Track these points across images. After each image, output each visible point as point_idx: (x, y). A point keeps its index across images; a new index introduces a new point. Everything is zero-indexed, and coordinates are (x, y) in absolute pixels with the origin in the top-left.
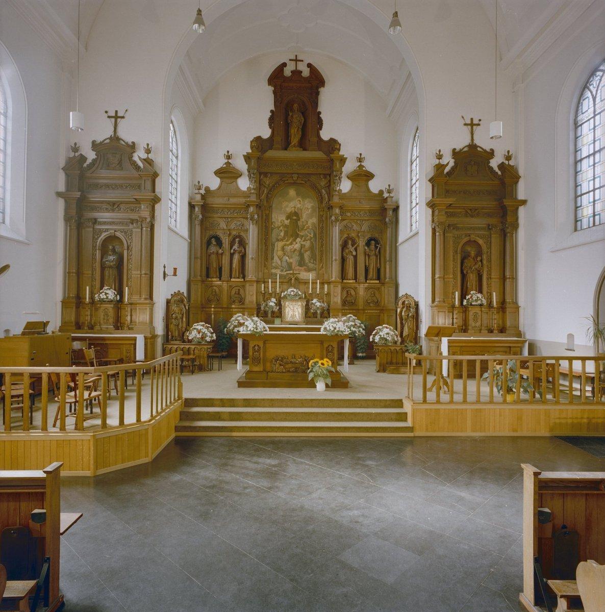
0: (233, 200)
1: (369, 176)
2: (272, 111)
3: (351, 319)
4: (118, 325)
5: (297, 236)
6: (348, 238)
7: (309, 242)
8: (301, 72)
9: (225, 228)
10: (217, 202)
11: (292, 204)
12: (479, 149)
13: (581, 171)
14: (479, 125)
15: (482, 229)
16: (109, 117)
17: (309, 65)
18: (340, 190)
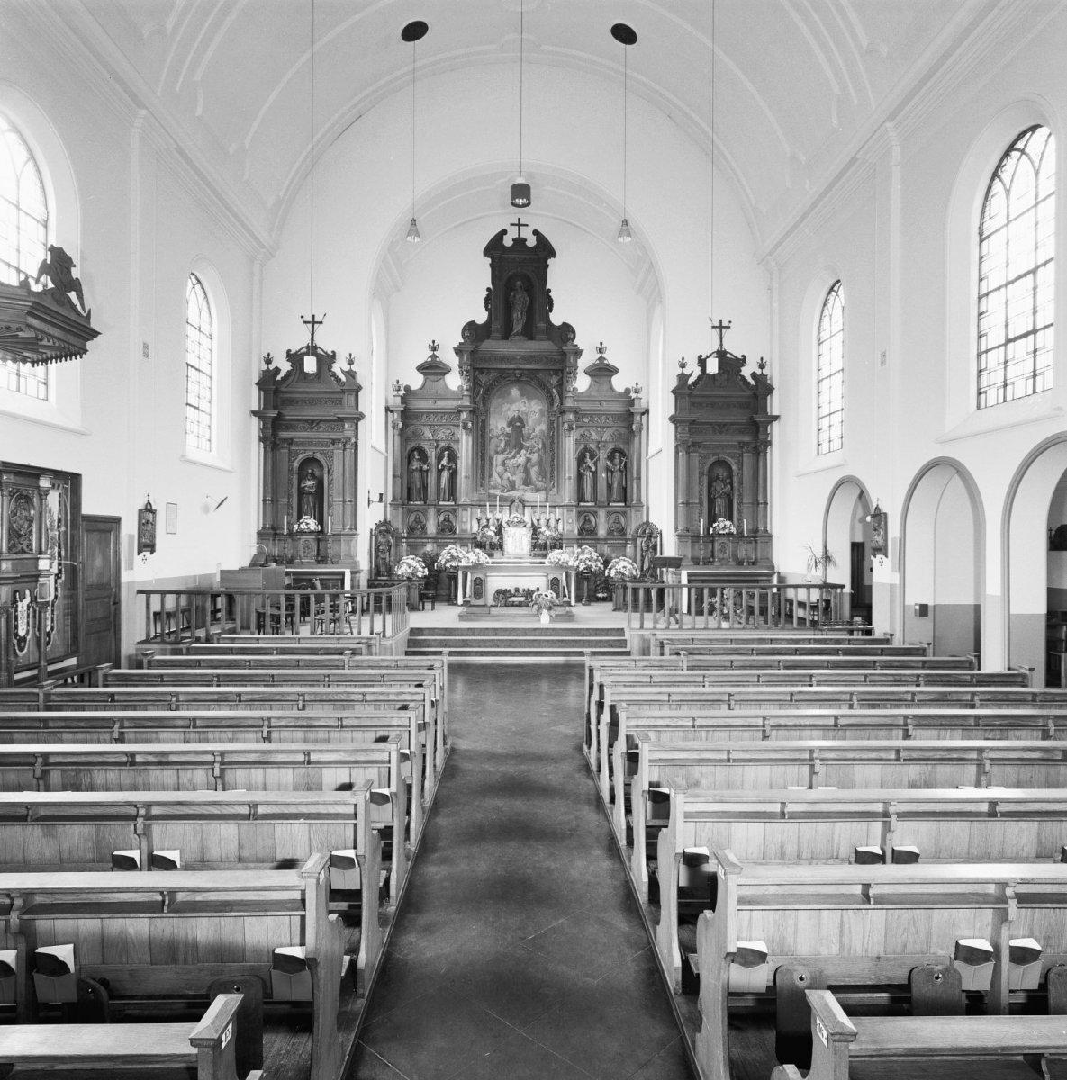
0: (441, 404)
1: (612, 371)
2: (488, 289)
3: (586, 551)
4: (322, 558)
5: (521, 447)
6: (586, 449)
7: (536, 454)
8: (526, 240)
9: (431, 438)
10: (419, 405)
11: (514, 407)
12: (728, 355)
13: (986, 311)
14: (728, 327)
15: (734, 446)
16: (305, 322)
17: (536, 233)
18: (575, 389)
